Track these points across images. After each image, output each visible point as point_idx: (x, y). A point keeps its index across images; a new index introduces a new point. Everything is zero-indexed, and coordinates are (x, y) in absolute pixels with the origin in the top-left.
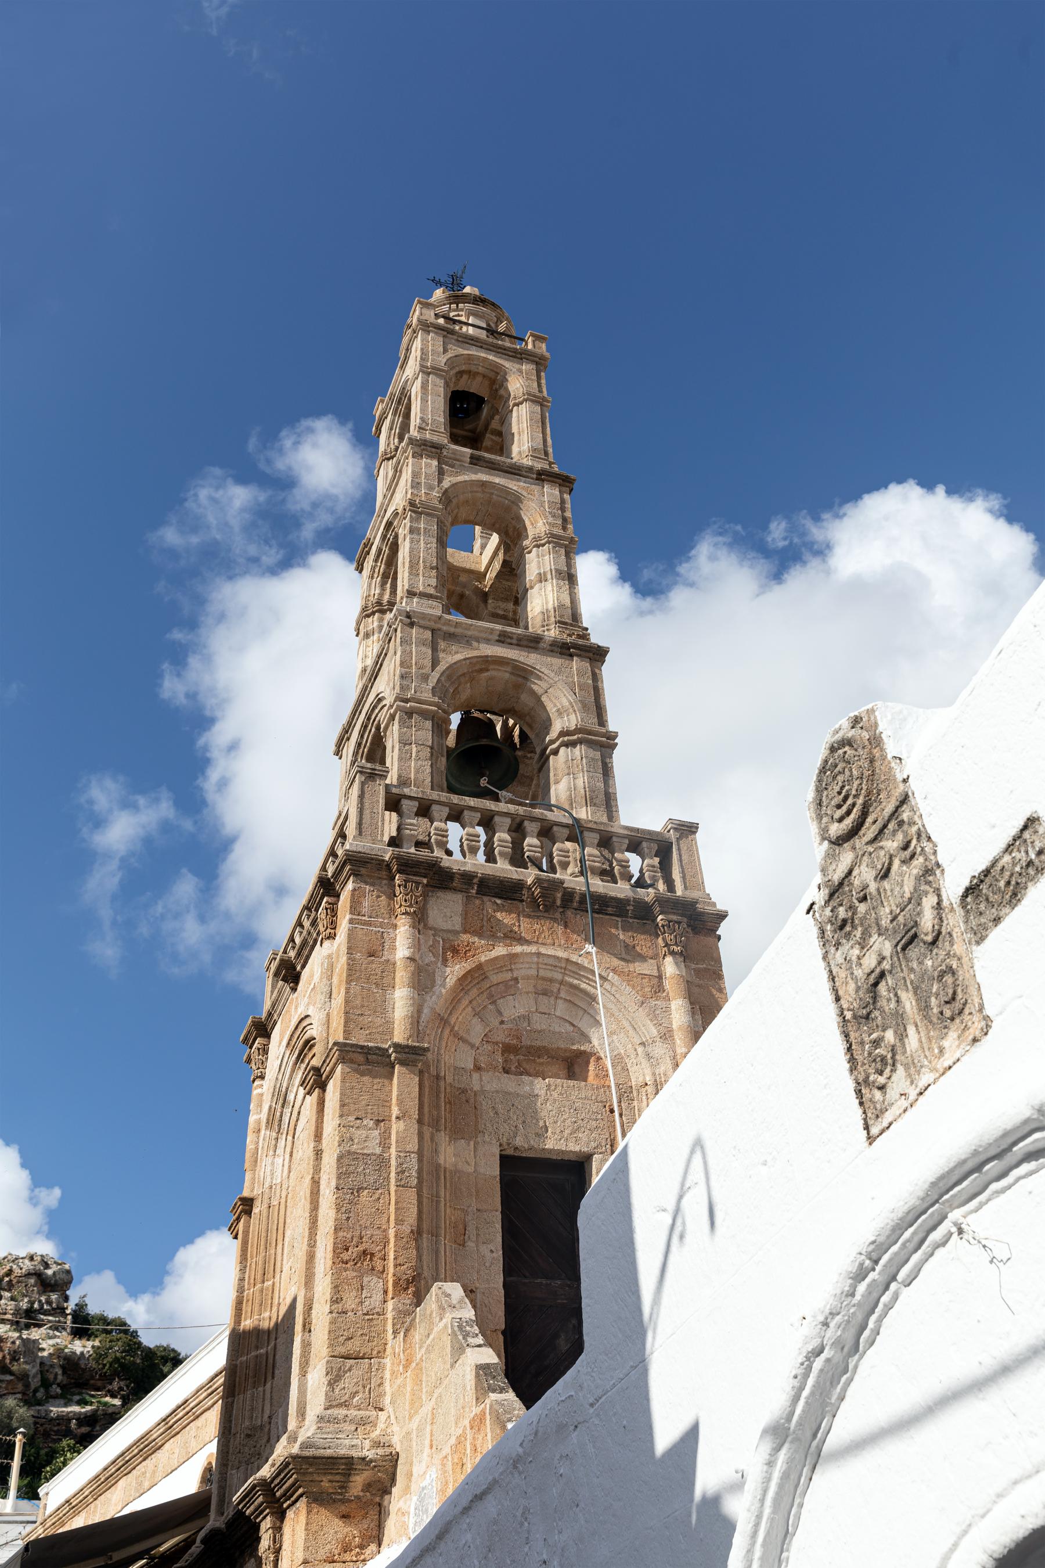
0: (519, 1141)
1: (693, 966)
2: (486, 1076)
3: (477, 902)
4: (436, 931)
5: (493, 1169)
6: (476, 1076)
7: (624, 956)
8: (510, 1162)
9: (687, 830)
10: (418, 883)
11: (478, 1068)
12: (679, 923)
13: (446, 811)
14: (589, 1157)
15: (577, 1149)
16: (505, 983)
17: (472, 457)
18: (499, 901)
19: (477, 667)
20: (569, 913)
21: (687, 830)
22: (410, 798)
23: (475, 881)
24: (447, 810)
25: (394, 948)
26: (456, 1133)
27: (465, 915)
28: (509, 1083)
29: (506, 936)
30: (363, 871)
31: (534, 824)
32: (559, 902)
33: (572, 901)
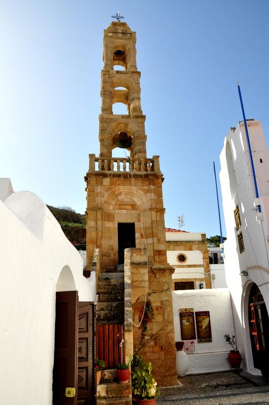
5: (117, 226)
8: (120, 225)
9: (158, 157)
11: (114, 209)
21: (158, 157)
26: (109, 221)
27: (110, 182)
28: (119, 211)
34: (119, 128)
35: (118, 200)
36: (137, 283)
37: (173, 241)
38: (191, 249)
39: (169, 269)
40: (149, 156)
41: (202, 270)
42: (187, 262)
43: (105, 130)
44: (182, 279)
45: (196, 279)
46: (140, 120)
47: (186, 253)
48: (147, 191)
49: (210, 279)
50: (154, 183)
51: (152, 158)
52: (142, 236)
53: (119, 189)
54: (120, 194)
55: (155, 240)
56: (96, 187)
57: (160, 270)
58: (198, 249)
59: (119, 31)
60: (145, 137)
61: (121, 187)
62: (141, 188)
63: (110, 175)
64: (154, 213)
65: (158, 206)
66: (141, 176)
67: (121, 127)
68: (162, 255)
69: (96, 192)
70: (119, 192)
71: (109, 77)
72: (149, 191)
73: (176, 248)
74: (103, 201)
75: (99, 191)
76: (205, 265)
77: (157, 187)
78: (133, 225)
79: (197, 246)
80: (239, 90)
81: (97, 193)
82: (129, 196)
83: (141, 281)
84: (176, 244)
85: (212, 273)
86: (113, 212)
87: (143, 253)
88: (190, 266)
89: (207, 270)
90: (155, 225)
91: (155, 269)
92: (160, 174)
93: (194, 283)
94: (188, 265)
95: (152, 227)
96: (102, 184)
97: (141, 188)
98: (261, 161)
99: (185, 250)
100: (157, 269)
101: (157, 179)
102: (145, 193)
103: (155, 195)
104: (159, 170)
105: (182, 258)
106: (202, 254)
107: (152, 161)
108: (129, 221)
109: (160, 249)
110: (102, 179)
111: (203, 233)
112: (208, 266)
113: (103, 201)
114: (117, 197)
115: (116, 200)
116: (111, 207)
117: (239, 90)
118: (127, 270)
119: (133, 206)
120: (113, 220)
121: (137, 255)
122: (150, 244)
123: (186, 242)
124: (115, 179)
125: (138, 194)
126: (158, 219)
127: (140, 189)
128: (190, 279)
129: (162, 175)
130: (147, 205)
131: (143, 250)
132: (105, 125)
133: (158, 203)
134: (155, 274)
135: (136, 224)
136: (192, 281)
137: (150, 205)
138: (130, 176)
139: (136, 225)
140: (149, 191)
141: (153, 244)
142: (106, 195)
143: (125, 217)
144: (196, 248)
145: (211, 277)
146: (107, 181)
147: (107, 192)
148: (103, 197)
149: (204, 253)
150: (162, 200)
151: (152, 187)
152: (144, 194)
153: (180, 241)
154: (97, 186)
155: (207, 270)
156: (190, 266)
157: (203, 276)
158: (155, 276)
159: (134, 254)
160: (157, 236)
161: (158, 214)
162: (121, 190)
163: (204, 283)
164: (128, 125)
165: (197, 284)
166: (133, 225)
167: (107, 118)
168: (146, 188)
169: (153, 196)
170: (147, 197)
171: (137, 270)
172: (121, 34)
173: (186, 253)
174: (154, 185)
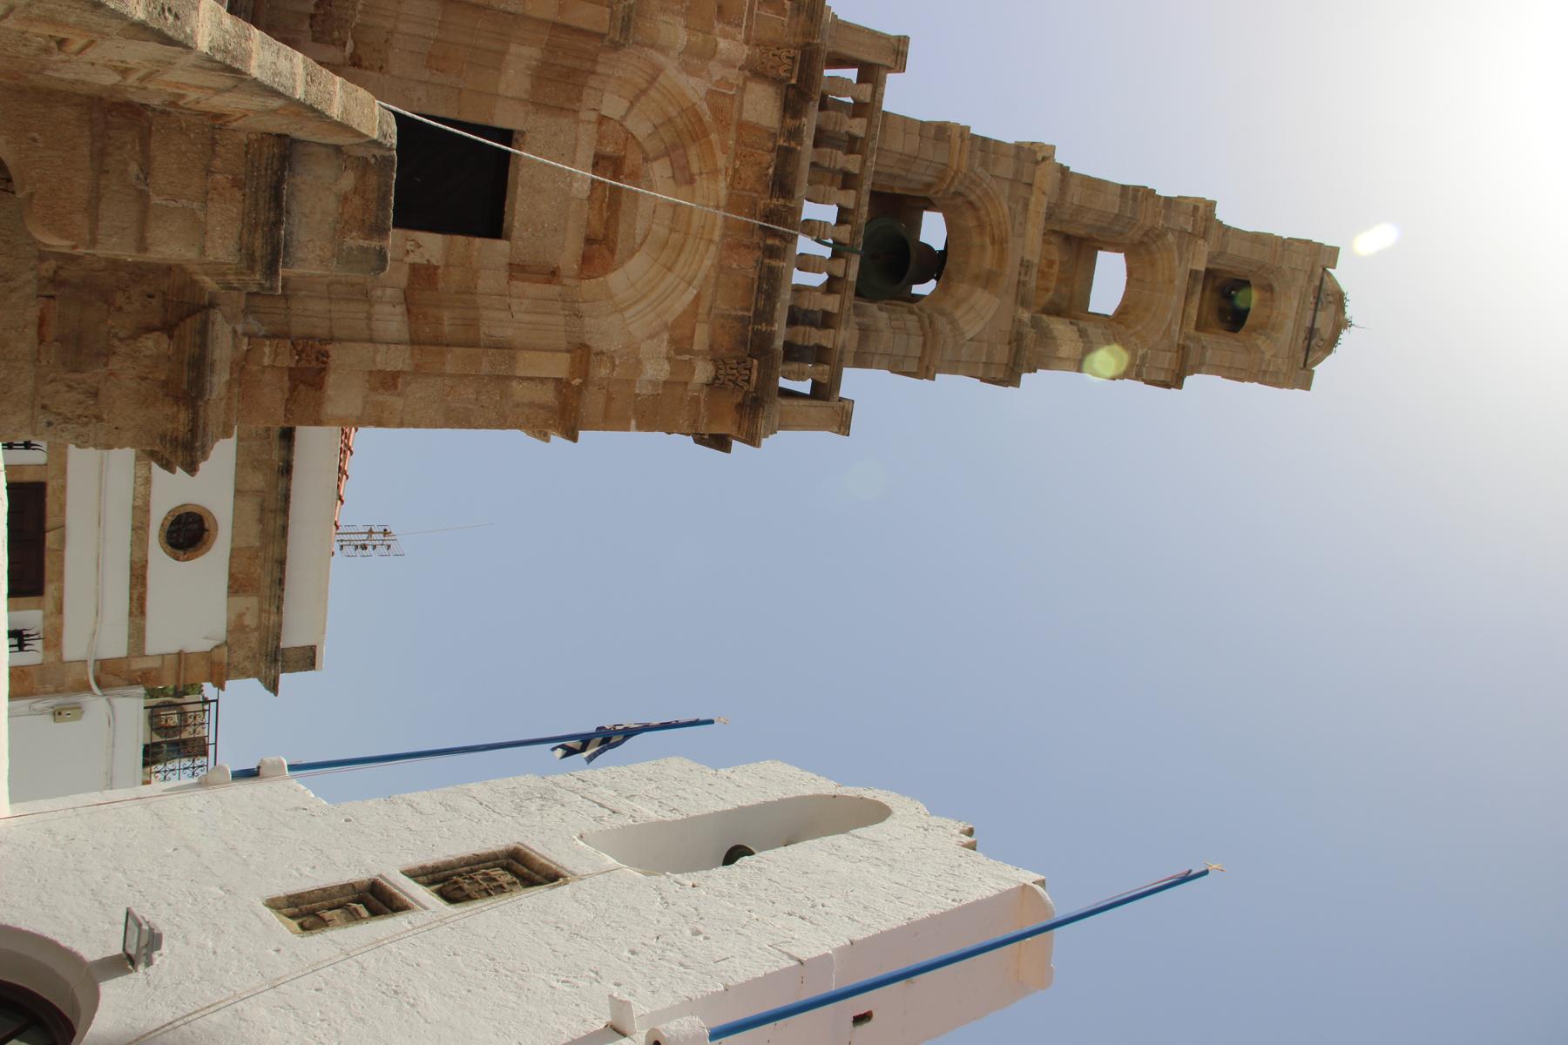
0: (650, 812)
1: (702, 396)
2: (592, 128)
3: (770, 145)
4: (742, 89)
5: (502, 119)
6: (593, 116)
7: (714, 311)
9: (843, 426)
10: (791, 71)
11: (602, 120)
12: (748, 381)
13: (825, 379)
14: (508, 238)
15: (517, 224)
16: (686, 167)
17: (1197, 272)
18: (771, 171)
19: (996, 232)
20: (758, 254)
21: (843, 426)
22: (864, 162)
23: (793, 144)
24: (851, 206)
25: (725, 37)
27: (756, 127)
29: (736, 171)
30: (803, 17)
31: (837, 305)
32: (769, 242)
33: (770, 257)
34: (976, 240)
35: (646, 159)
36: (134, 168)
37: (288, 490)
38: (237, 585)
39: (193, 431)
40: (855, 382)
41: (115, 645)
42: (158, 558)
43: (984, 164)
44: (62, 526)
45: (60, 610)
46: (1002, 354)
47: (215, 562)
48: (680, 345)
49: (57, 692)
50: (722, 386)
51: (844, 392)
52: (423, 275)
53: (714, 172)
54: (684, 178)
55: (397, 359)
56: (741, 37)
57: (199, 365)
58: (237, 628)
59: (1320, 316)
60: (924, 370)
61: (722, 186)
62: (703, 310)
63: (795, 134)
64: (558, 366)
65: (593, 401)
66: (764, 315)
67: (983, 247)
68: (293, 389)
69: (718, 27)
70: (695, 168)
71: (1182, 232)
72: (679, 352)
73: (251, 507)
74: (659, 58)
75: (723, 44)
76: (139, 664)
77: (696, 400)
78: (492, 224)
79: (250, 621)
80: (1187, 878)
81: (708, 32)
82: (660, 230)
83: (143, 196)
84: (271, 503)
85: (95, 704)
86: (584, 115)
87: (355, 241)
88: (138, 576)
89: (110, 676)
90: (485, 368)
91: (204, 331)
92: (762, 423)
93: (34, 599)
94: (144, 567)
95: (475, 345)
96: (756, 72)
97: (703, 310)
98: (860, 1019)
99: (234, 554)
100: (203, 345)
101: (740, 407)
102: (674, 326)
103: (654, 383)
104: (783, 427)
105: (187, 533)
106: (206, 646)
107: (824, 391)
108: (521, 207)
109: (331, 379)
110: (776, 81)
111: (325, 656)
112: (132, 682)
113: (659, 58)
114: (667, 152)
115: (649, 146)
116: (613, 106)
117: (1187, 878)
118: (284, 65)
119: (600, 249)
120: (538, 104)
121: (345, 199)
122: (369, 318)
123: (282, 563)
124: (769, 158)
125: (654, 298)
126: (520, 391)
127: (698, 297)
128: (61, 573)
129: (753, 440)
130: (606, 332)
131: (375, 244)
132: (1006, 168)
133: (610, 399)
134: (168, 329)
135: (501, 245)
136: (50, 589)
137: (603, 346)
138: (772, 252)
139: (498, 249)
140: (679, 352)
141: (371, 340)
142: (694, 89)
143: (551, 174)
144: (241, 616)
145: (73, 699)
146: (762, 106)
147: (710, 92)
148: (686, 68)
149: (207, 656)
150: (627, 429)
151: (703, 372)
152: (670, 318)
153: (285, 528)
154: (747, 42)
155: (110, 676)
156: (138, 576)
157: (74, 647)
158: (149, 329)
159: (348, 181)
160: (419, 371)
161: (547, 395)
162: (702, 184)
163: (34, 655)
164: (985, 287)
165: (33, 618)
166: (492, 224)
167: (1030, 185)
168: (701, 338)
169: (656, 370)
170: (651, 337)
171: (236, 183)
172: (1308, 324)
173: (215, 562)
174: (713, 385)
